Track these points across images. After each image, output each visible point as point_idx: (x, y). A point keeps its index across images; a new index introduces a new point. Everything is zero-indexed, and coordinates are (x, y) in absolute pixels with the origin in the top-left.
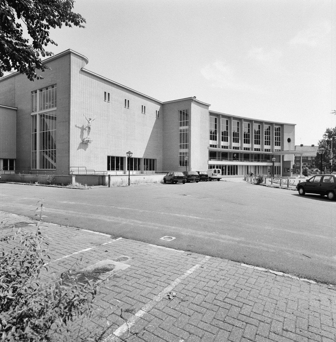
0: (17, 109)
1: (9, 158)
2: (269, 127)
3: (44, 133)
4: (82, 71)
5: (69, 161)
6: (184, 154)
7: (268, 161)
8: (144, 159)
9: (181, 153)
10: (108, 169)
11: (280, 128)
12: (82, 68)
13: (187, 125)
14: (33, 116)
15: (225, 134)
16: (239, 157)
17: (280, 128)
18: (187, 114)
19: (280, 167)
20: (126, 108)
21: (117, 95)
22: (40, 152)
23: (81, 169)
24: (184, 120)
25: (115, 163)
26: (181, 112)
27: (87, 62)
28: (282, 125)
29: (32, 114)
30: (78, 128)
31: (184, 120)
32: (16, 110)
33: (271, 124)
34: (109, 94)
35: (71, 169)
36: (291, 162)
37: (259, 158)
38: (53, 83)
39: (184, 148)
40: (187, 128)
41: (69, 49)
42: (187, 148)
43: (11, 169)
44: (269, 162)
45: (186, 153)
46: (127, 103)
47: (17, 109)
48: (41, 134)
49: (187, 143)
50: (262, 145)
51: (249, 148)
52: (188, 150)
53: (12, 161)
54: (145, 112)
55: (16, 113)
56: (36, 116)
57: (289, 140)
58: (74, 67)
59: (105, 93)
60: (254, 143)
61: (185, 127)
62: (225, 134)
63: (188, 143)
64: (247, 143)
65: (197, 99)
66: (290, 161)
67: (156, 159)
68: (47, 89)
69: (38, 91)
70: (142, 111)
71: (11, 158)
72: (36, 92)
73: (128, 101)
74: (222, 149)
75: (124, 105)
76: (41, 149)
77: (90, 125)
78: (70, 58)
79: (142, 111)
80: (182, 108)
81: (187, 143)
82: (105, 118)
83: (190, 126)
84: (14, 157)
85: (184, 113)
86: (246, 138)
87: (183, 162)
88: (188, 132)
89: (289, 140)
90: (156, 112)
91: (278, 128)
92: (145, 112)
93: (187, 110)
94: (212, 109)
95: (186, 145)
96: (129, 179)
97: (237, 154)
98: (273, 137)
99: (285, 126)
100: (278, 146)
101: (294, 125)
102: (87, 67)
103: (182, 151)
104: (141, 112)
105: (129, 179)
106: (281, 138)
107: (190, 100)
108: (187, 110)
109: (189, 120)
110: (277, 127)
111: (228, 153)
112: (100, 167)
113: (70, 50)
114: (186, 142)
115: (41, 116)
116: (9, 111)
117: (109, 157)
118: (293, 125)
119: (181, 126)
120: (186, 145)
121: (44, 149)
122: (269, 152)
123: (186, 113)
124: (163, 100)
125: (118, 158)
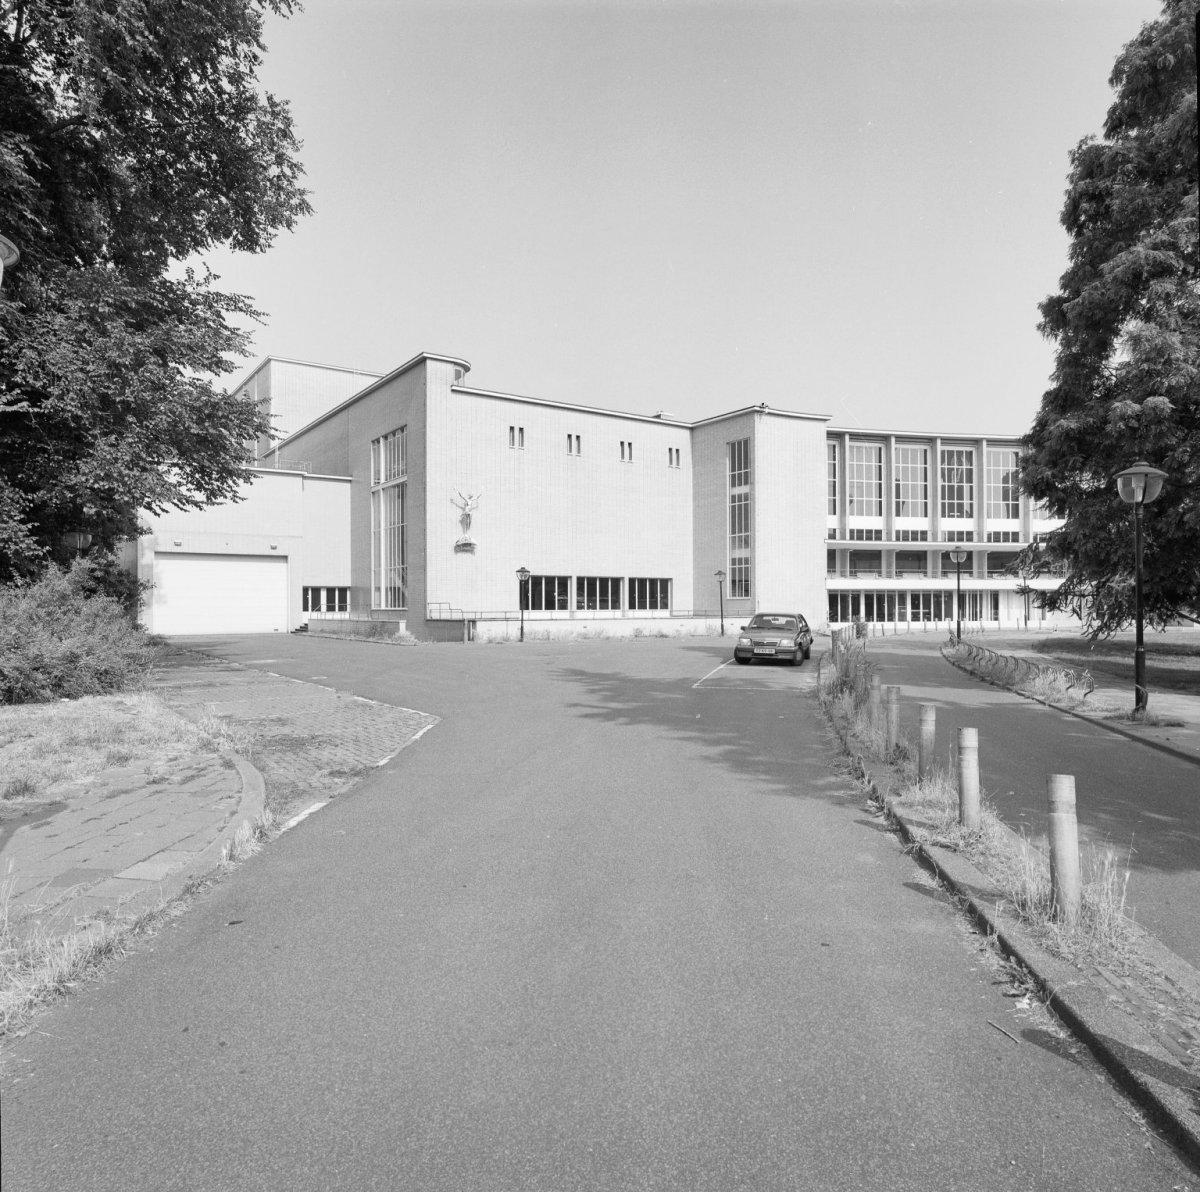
1: (558, 574)
6: (740, 560)
15: (740, 479)
21: (601, 435)
25: (540, 592)
30: (454, 506)
35: (429, 607)
38: (402, 423)
43: (342, 608)
45: (747, 561)
46: (574, 440)
50: (933, 517)
51: (879, 532)
53: (343, 591)
54: (631, 458)
62: (740, 479)
64: (862, 514)
65: (773, 405)
68: (394, 435)
69: (382, 440)
70: (623, 457)
71: (342, 584)
72: (379, 442)
74: (851, 542)
79: (623, 457)
80: (735, 433)
84: (346, 582)
86: (956, 501)
92: (631, 458)
93: (746, 442)
96: (722, 626)
97: (970, 554)
105: (722, 626)
111: (883, 554)
117: (305, 590)
125: (653, 582)
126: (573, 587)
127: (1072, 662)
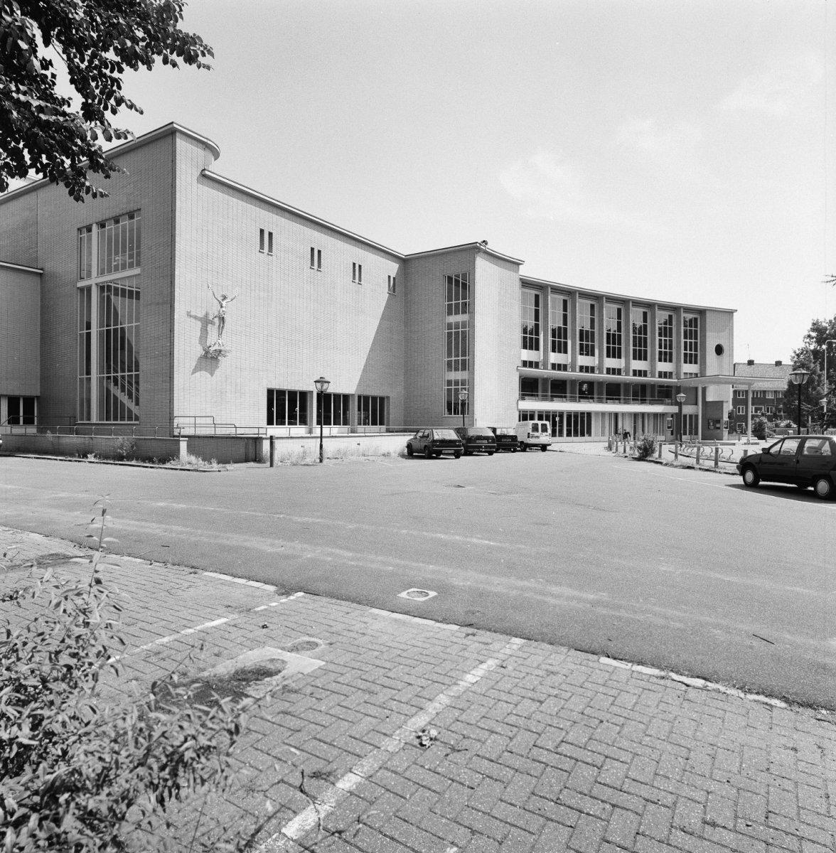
0: (41, 272)
1: (23, 393)
2: (670, 317)
3: (108, 331)
4: (204, 176)
5: (171, 401)
6: (457, 383)
7: (667, 401)
8: (359, 397)
9: (449, 383)
10: (270, 422)
11: (696, 319)
12: (204, 170)
13: (464, 312)
14: (81, 289)
15: (560, 333)
16: (595, 391)
17: (696, 319)
18: (464, 285)
19: (697, 416)
20: (312, 271)
21: (291, 236)
22: (101, 380)
23: (202, 421)
24: (457, 299)
25: (285, 406)
26: (450, 279)
27: (216, 154)
28: (702, 312)
29: (80, 284)
30: (193, 320)
31: (457, 299)
32: (41, 274)
33: (675, 309)
34: (270, 234)
35: (176, 421)
36: (724, 404)
37: (644, 394)
38: (132, 207)
39: (457, 369)
40: (465, 320)
41: (172, 123)
42: (465, 369)
43: (28, 421)
44: (668, 404)
45: (463, 383)
46: (316, 257)
47: (41, 272)
48: (101, 333)
49: (466, 356)
50: (651, 361)
51: (619, 370)
52: (469, 374)
53: (29, 401)
54: (360, 280)
55: (39, 281)
56: (89, 289)
57: (719, 350)
58: (183, 167)
59: (262, 231)
60: (631, 357)
61: (460, 318)
62: (560, 333)
63: (467, 358)
64: (615, 357)
65: (491, 246)
66: (722, 402)
67: (388, 397)
68: (117, 222)
69: (94, 228)
70: (354, 278)
71: (28, 393)
72: (89, 229)
73: (319, 252)
74: (552, 371)
75: (309, 262)
76: (101, 372)
77: (223, 311)
78: (174, 144)
79: (354, 278)
80: (454, 269)
81: (466, 356)
82: (262, 294)
83: (472, 313)
84: (34, 391)
85: (457, 282)
86: (611, 345)
87: (457, 404)
88: (467, 329)
89: (719, 350)
90: (387, 280)
91: (691, 320)
92: (360, 280)
93: (464, 275)
94: (526, 271)
95: (464, 362)
96: (321, 446)
97: (591, 384)
98: (680, 341)
99: (708, 314)
100: (693, 365)
101: (732, 313)
102: (217, 168)
103: (453, 376)
104: (352, 279)
105: (321, 446)
106: (699, 343)
107: (473, 250)
108: (464, 275)
109: (471, 299)
110: (690, 316)
111: (568, 382)
112: (249, 416)
113: (175, 125)
114: (464, 355)
115: (102, 288)
116: (23, 276)
117: (270, 392)
118: (730, 313)
119: (450, 313)
120: (464, 362)
121: (109, 372)
122: (669, 378)
123: (462, 283)
124: (405, 250)
125: (292, 394)
126: (353, 406)
127: (307, 534)
